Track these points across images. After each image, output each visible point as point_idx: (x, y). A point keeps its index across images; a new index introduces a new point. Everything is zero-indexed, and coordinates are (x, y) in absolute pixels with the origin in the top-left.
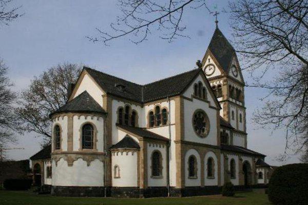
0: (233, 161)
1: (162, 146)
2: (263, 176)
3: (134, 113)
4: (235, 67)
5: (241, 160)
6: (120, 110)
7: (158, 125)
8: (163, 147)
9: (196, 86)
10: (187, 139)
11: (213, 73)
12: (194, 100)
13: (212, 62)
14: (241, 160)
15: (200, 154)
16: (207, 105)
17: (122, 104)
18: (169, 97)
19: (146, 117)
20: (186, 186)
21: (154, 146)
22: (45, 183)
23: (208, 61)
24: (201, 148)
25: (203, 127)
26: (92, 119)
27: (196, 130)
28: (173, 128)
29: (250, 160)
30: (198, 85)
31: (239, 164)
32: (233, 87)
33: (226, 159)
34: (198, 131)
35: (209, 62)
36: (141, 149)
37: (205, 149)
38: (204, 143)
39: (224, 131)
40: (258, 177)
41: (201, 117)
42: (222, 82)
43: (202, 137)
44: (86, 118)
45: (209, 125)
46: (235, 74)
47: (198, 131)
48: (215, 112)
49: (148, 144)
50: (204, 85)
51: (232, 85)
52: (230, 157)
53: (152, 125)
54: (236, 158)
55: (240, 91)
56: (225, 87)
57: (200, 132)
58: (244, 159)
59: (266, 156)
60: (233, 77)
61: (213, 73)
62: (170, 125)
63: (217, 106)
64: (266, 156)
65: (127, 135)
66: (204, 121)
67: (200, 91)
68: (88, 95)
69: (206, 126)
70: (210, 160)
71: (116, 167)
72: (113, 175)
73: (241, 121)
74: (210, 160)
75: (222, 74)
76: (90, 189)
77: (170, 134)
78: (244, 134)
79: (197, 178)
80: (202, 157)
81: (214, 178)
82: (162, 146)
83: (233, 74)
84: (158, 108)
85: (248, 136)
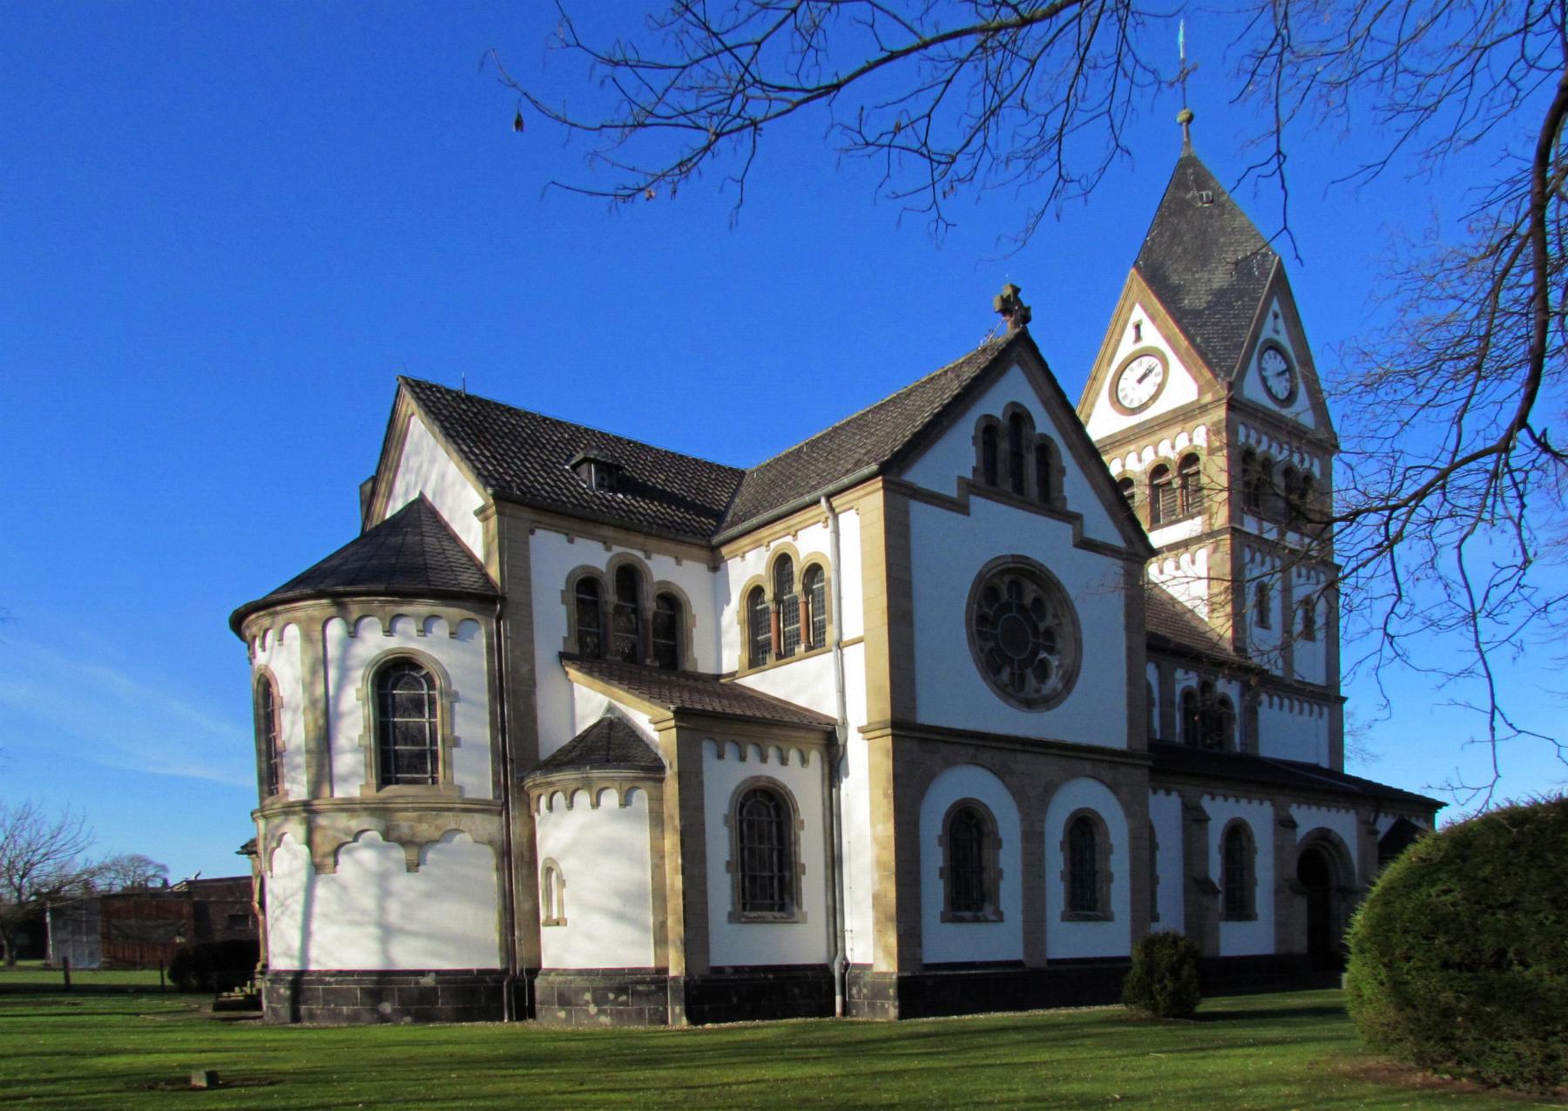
0: (1237, 834)
3: (672, 603)
4: (1285, 357)
5: (1286, 824)
6: (585, 587)
7: (785, 655)
9: (988, 431)
10: (928, 715)
11: (1154, 398)
12: (977, 503)
13: (1152, 337)
14: (1286, 824)
15: (1018, 794)
16: (1065, 531)
17: (595, 555)
18: (829, 497)
20: (929, 958)
21: (743, 758)
22: (1305, 951)
23: (1130, 332)
25: (1043, 655)
27: (997, 671)
28: (855, 657)
29: (1343, 824)
31: (1279, 850)
33: (1194, 819)
34: (1005, 675)
35: (1138, 338)
36: (671, 774)
38: (1034, 734)
39: (1206, 686)
41: (1028, 599)
42: (1200, 438)
43: (1030, 704)
45: (1078, 643)
46: (1280, 387)
47: (1005, 675)
48: (1112, 568)
49: (708, 749)
50: (1043, 424)
52: (1221, 811)
53: (757, 656)
54: (1258, 815)
55: (1308, 478)
56: (1221, 460)
57: (1019, 681)
58: (1308, 818)
60: (1266, 401)
61: (1154, 398)
62: (840, 645)
63: (1127, 540)
64: (1440, 805)
65: (610, 709)
66: (1049, 621)
67: (1017, 456)
68: (434, 514)
69: (1059, 644)
70: (1083, 828)
71: (549, 870)
72: (542, 917)
73: (1308, 634)
74: (1083, 828)
75: (1201, 392)
76: (428, 981)
77: (842, 692)
78: (1328, 698)
79: (1107, 917)
80: (1033, 807)
81: (1107, 917)
82: (793, 755)
83: (1269, 391)
84: (783, 562)
85: (1346, 706)
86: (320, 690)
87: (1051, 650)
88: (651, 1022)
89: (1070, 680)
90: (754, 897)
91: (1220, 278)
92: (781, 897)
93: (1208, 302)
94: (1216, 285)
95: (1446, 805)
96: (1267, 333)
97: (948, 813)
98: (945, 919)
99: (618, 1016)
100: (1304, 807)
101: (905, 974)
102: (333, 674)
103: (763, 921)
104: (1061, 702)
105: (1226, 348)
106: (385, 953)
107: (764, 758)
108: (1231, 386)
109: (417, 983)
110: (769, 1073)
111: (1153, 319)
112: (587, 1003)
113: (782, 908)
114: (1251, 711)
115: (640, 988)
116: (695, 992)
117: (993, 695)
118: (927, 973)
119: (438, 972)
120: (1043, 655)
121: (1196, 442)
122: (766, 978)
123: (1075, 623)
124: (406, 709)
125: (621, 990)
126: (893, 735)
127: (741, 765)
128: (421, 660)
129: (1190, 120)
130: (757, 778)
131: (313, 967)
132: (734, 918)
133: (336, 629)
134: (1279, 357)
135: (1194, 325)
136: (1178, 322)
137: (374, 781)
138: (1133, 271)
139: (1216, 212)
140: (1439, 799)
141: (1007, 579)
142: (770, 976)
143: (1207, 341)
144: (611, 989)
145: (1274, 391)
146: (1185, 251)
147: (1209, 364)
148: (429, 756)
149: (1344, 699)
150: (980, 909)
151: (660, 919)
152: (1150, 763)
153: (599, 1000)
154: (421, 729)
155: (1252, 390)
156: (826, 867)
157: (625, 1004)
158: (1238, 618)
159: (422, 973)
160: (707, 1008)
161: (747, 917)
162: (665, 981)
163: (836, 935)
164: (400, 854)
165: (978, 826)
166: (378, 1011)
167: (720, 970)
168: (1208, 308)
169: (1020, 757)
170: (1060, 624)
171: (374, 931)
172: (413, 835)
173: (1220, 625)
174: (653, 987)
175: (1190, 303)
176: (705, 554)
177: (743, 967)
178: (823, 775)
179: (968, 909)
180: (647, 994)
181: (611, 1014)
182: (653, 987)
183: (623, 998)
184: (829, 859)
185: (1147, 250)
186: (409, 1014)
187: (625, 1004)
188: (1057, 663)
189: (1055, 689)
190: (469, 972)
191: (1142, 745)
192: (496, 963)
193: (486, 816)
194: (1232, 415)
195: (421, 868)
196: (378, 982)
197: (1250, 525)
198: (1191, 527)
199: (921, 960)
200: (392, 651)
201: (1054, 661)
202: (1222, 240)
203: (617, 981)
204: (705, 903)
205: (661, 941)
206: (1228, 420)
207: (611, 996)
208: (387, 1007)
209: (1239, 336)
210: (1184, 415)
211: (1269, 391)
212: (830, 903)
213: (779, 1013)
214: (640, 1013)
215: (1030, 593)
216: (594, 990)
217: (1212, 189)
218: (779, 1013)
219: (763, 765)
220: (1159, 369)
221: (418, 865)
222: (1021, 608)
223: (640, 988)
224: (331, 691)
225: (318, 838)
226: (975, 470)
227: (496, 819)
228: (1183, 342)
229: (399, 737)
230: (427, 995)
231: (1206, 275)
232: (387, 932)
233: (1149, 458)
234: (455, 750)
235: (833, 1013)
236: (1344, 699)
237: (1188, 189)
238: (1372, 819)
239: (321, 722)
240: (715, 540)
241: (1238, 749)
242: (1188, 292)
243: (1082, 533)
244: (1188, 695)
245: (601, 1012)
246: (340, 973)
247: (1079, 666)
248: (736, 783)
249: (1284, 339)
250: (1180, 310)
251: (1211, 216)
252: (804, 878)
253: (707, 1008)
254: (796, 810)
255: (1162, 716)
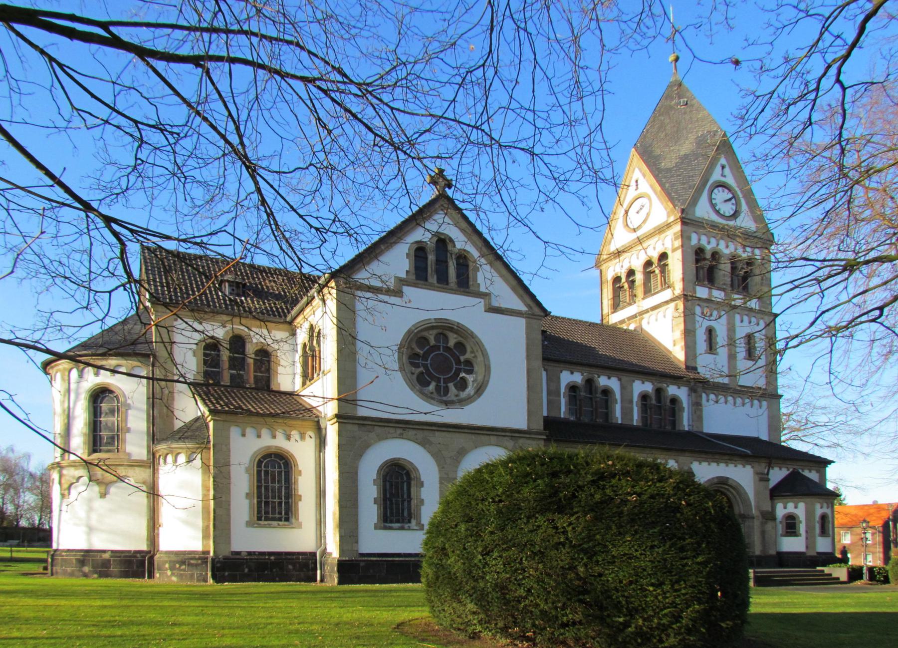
1: (295, 434)
2: (802, 528)
6: (211, 347)
8: (302, 436)
9: (420, 251)
11: (644, 221)
12: (406, 289)
15: (437, 456)
16: (480, 303)
17: (577, 378)
19: (686, 410)
21: (259, 436)
23: (718, 169)
24: (439, 437)
25: (463, 375)
26: (796, 507)
30: (655, 260)
32: (715, 255)
37: (460, 440)
40: (780, 529)
41: (451, 343)
43: (448, 404)
44: (785, 508)
50: (460, 241)
51: (709, 248)
56: (679, 254)
59: (830, 462)
60: (714, 217)
61: (644, 221)
64: (830, 462)
66: (468, 356)
69: (476, 369)
75: (668, 216)
76: (106, 556)
83: (717, 212)
86: (66, 405)
87: (470, 372)
88: (198, 580)
89: (480, 391)
90: (267, 513)
91: (686, 147)
92: (287, 513)
93: (676, 164)
94: (682, 153)
95: (833, 462)
96: (716, 176)
97: (381, 468)
98: (376, 527)
99: (180, 576)
100: (705, 464)
101: (344, 559)
102: (73, 396)
103: (270, 526)
104: (471, 402)
105: (684, 188)
106: (89, 540)
107: (288, 438)
108: (683, 211)
109: (101, 557)
110: (77, 603)
111: (644, 176)
112: (167, 570)
113: (287, 519)
114: (697, 405)
115: (192, 562)
116: (218, 565)
117: (421, 401)
118: (360, 559)
119: (113, 551)
120: (463, 375)
121: (666, 246)
122: (269, 559)
123: (485, 355)
124: (106, 414)
125: (183, 562)
126: (339, 422)
127: (243, 439)
128: (113, 389)
129: (677, 59)
130: (269, 447)
131: (61, 547)
132: (249, 524)
133: (74, 373)
134: (726, 191)
135: (665, 177)
136: (655, 177)
137: (87, 451)
138: (633, 150)
139: (688, 110)
140: (829, 458)
141: (435, 332)
142: (272, 558)
143: (672, 186)
144: (178, 562)
145: (722, 212)
146: (666, 135)
147: (672, 200)
148: (116, 438)
149: (781, 396)
150: (409, 522)
151: (206, 524)
152: (545, 437)
153: (172, 568)
154: (113, 424)
155: (703, 210)
156: (317, 497)
157: (184, 570)
158: (690, 347)
159: (104, 551)
160: (227, 574)
161: (260, 524)
162: (207, 558)
163: (321, 536)
164: (96, 489)
165: (408, 474)
166: (82, 571)
167: (239, 553)
168: (676, 166)
169: (437, 433)
170: (475, 357)
171: (84, 529)
172: (103, 479)
173: (679, 354)
174: (200, 562)
175: (665, 165)
176: (286, 326)
177: (254, 552)
178: (316, 445)
179: (398, 521)
180: (197, 565)
181: (177, 576)
182: (200, 562)
183: (183, 567)
184: (318, 493)
185: (643, 136)
186: (96, 573)
187: (184, 570)
188: (472, 379)
189: (469, 394)
190: (129, 551)
191: (539, 425)
192: (144, 547)
193: (142, 469)
194: (685, 227)
195: (107, 496)
196: (83, 556)
197: (702, 292)
198: (667, 295)
199: (357, 551)
200: (98, 385)
201: (470, 378)
202: (690, 126)
203: (180, 558)
204: (229, 515)
205: (205, 536)
206: (682, 231)
207: (178, 566)
208: (86, 569)
209: (693, 181)
210: (660, 230)
211: (717, 212)
212: (318, 517)
213: (277, 579)
214: (192, 576)
215: (452, 340)
216: (170, 562)
217: (688, 97)
218: (277, 579)
219: (274, 440)
220: (647, 206)
221: (105, 495)
222: (447, 349)
223: (192, 562)
224: (71, 406)
225: (63, 481)
226: (407, 272)
227: (148, 470)
228: (658, 188)
229: (102, 428)
230: (106, 564)
231: (677, 147)
232: (91, 529)
233: (643, 259)
234: (127, 434)
235: (315, 580)
236: (781, 396)
237: (672, 99)
238: (766, 471)
239: (66, 421)
240: (289, 318)
241: (686, 429)
242: (665, 159)
243: (490, 304)
244: (644, 397)
245: (173, 574)
246: (69, 550)
247: (488, 381)
248: (255, 449)
249: (730, 180)
250: (660, 170)
251: (685, 113)
252: (300, 504)
253: (227, 574)
254: (296, 465)
255: (622, 408)
